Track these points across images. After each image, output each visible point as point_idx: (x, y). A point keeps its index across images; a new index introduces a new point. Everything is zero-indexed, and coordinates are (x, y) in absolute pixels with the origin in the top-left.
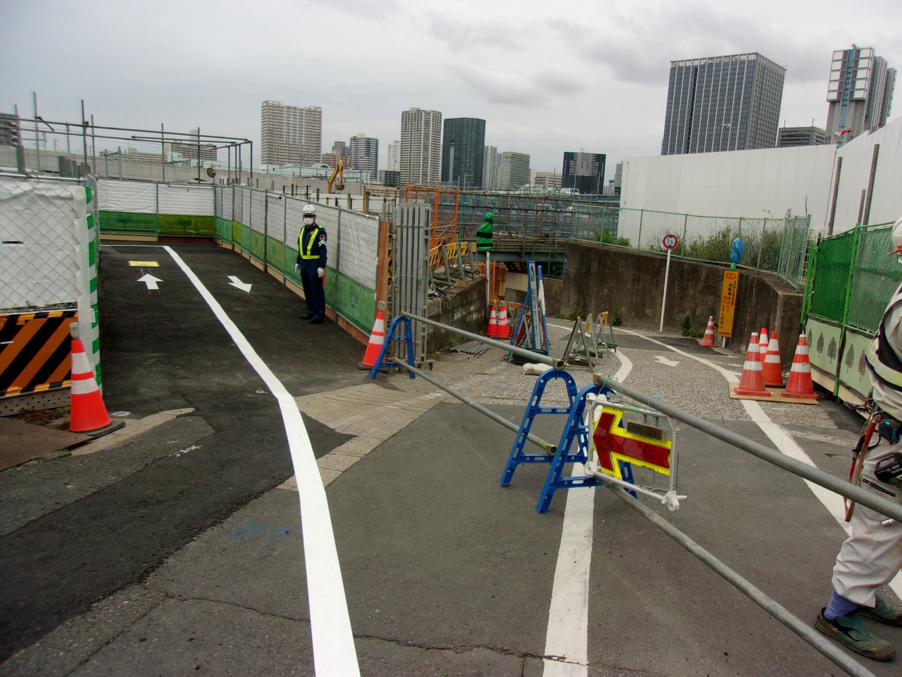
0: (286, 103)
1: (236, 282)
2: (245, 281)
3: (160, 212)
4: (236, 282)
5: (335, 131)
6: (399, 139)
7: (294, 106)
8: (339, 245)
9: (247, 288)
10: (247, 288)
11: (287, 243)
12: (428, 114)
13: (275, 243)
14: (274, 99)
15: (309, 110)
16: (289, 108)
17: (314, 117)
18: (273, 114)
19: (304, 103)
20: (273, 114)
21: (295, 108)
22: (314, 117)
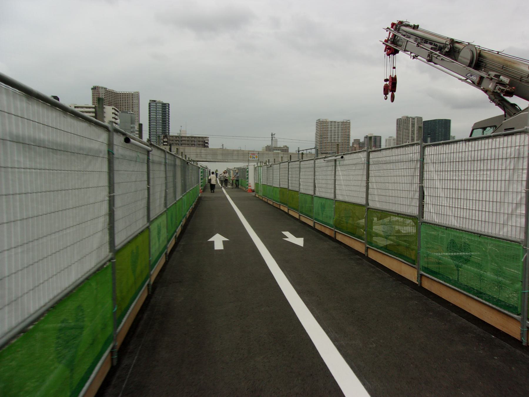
0: (330, 119)
1: (291, 238)
2: (297, 236)
3: (339, 198)
4: (291, 238)
5: (357, 133)
6: (394, 136)
7: (334, 120)
8: (148, 184)
9: (300, 242)
10: (300, 242)
11: (427, 217)
12: (413, 119)
13: (466, 236)
14: (323, 118)
15: (343, 123)
16: (331, 122)
17: (346, 126)
18: (323, 127)
19: (339, 119)
20: (323, 127)
21: (335, 122)
22: (346, 126)
